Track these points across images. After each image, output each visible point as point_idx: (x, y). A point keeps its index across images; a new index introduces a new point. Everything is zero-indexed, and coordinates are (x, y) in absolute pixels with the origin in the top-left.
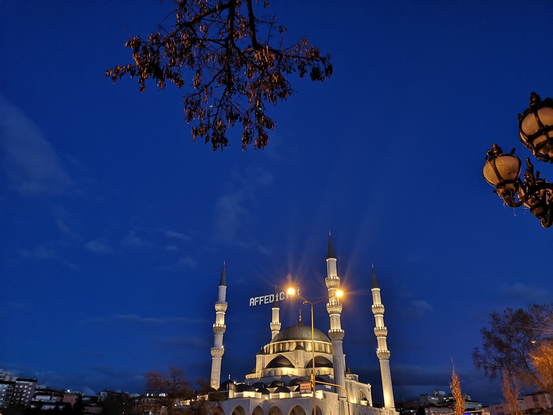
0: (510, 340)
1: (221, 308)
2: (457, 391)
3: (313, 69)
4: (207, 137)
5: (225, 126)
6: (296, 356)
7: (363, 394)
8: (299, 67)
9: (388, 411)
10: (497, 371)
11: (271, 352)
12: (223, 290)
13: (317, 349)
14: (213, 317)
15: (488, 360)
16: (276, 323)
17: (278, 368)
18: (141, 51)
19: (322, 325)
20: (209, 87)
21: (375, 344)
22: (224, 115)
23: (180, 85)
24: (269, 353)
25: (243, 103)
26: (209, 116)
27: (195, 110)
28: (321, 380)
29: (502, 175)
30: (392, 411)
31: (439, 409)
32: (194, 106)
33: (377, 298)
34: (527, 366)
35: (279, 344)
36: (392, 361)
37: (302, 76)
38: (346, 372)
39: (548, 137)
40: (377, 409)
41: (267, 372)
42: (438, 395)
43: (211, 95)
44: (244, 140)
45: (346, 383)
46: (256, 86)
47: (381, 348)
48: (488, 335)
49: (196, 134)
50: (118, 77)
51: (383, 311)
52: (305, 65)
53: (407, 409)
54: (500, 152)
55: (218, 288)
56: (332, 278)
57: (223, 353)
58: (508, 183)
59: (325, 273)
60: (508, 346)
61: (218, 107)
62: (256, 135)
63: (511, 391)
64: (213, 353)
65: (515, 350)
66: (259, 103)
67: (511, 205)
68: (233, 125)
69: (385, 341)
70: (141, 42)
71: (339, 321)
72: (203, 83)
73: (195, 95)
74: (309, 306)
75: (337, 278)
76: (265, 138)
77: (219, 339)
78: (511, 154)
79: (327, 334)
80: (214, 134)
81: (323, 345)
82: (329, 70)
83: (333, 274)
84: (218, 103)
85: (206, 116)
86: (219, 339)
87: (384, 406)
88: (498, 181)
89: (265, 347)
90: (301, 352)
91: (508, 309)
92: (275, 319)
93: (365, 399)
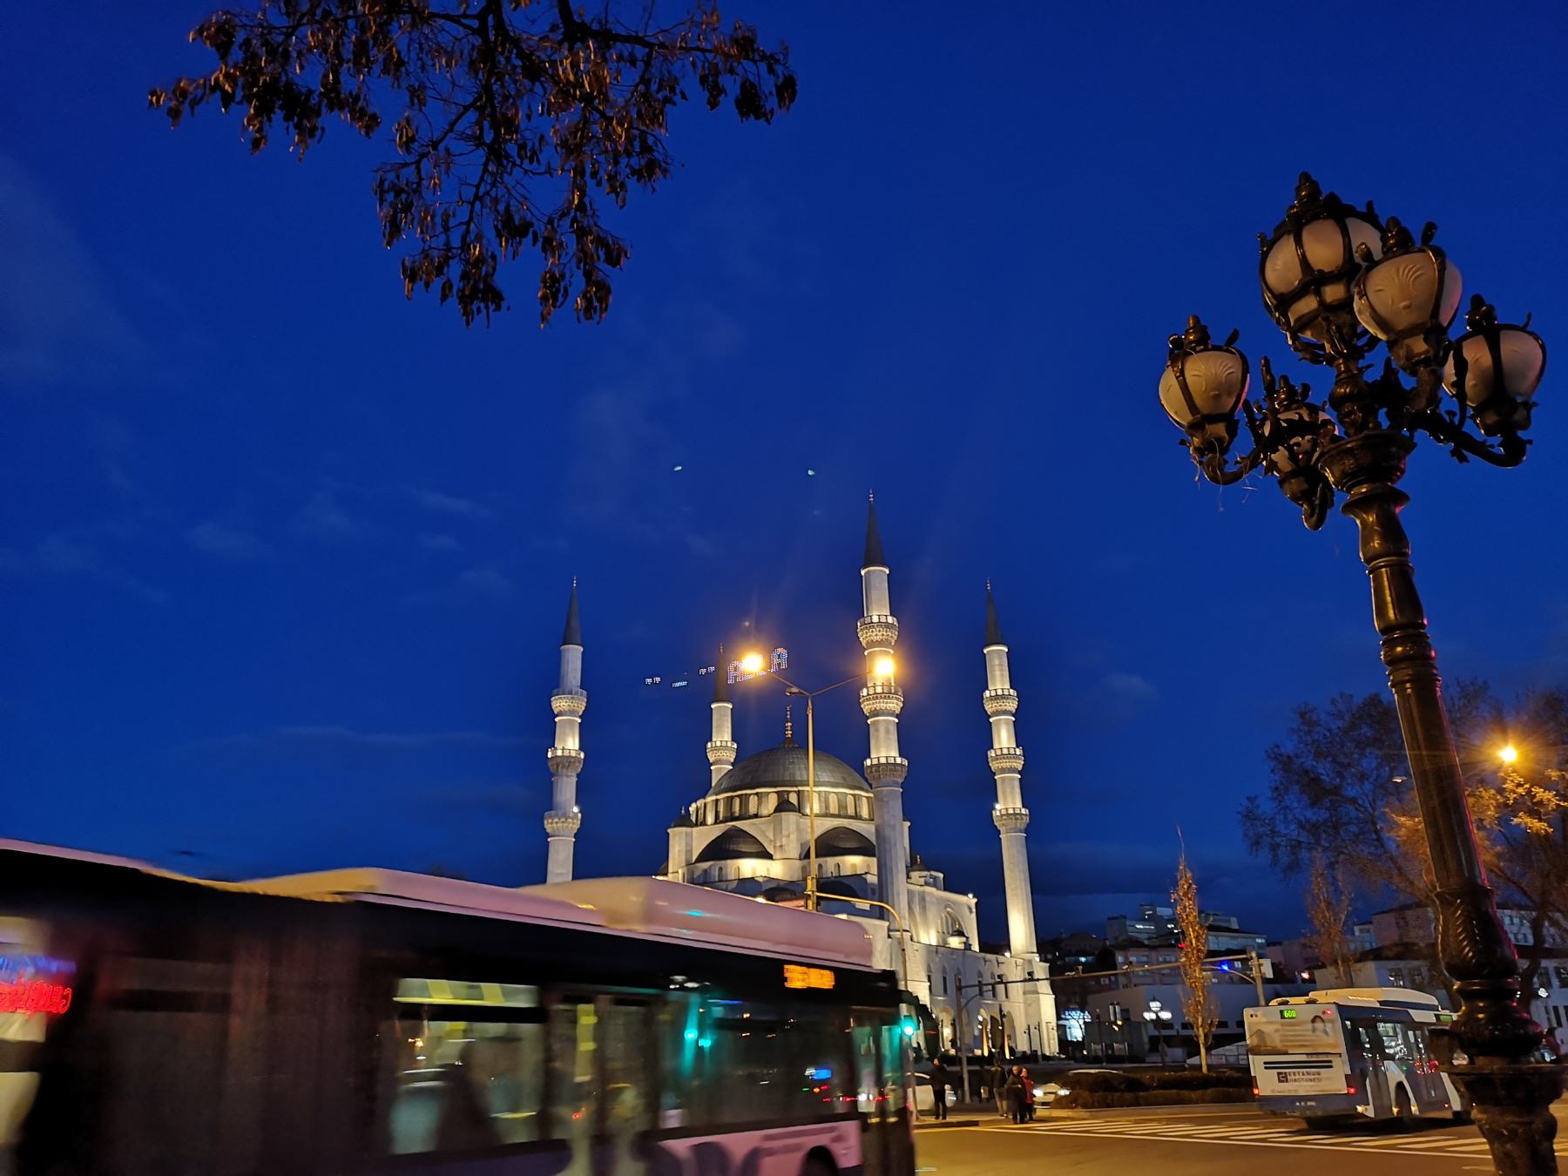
0: (1340, 775)
1: (568, 707)
2: (1185, 907)
3: (743, 86)
4: (447, 286)
5: (493, 257)
6: (778, 829)
7: (954, 920)
8: (703, 80)
9: (1020, 961)
10: (1304, 854)
11: (710, 819)
12: (573, 656)
13: (833, 809)
14: (549, 735)
15: (1281, 827)
16: (722, 745)
17: (729, 862)
18: (237, 54)
19: (845, 744)
20: (442, 146)
21: (990, 793)
22: (488, 223)
23: (368, 129)
24: (704, 823)
25: (543, 192)
26: (446, 229)
27: (407, 208)
28: (840, 888)
29: (1198, 401)
30: (1030, 962)
31: (1154, 954)
32: (402, 200)
33: (998, 673)
34: (1379, 839)
35: (730, 800)
36: (1033, 835)
37: (713, 104)
38: (911, 867)
39: (1322, 303)
40: (989, 956)
41: (697, 874)
42: (1153, 919)
43: (448, 168)
44: (545, 298)
45: (910, 893)
46: (571, 149)
47: (1005, 802)
48: (1285, 764)
49: (412, 276)
50: (186, 107)
51: (1012, 706)
52: (717, 74)
53: (1071, 954)
54: (1204, 341)
55: (560, 652)
56: (875, 619)
57: (577, 825)
58: (1210, 423)
59: (857, 609)
60: (1336, 791)
61: (472, 204)
62: (578, 281)
63: (1329, 904)
64: (549, 826)
65: (1354, 801)
66: (580, 198)
67: (1214, 479)
68: (515, 254)
69: (1017, 784)
70: (234, 27)
71: (894, 736)
72: (424, 136)
73: (405, 165)
74: (799, 703)
75: (890, 619)
76: (603, 289)
77: (567, 789)
78: (1229, 345)
79: (860, 769)
80: (465, 276)
81: (850, 800)
82: (787, 89)
83: (879, 610)
84: (469, 193)
85: (439, 229)
86: (567, 789)
87: (1009, 949)
88: (1190, 418)
89: (692, 808)
90: (790, 818)
91: (1342, 695)
92: (721, 732)
93: (960, 933)
